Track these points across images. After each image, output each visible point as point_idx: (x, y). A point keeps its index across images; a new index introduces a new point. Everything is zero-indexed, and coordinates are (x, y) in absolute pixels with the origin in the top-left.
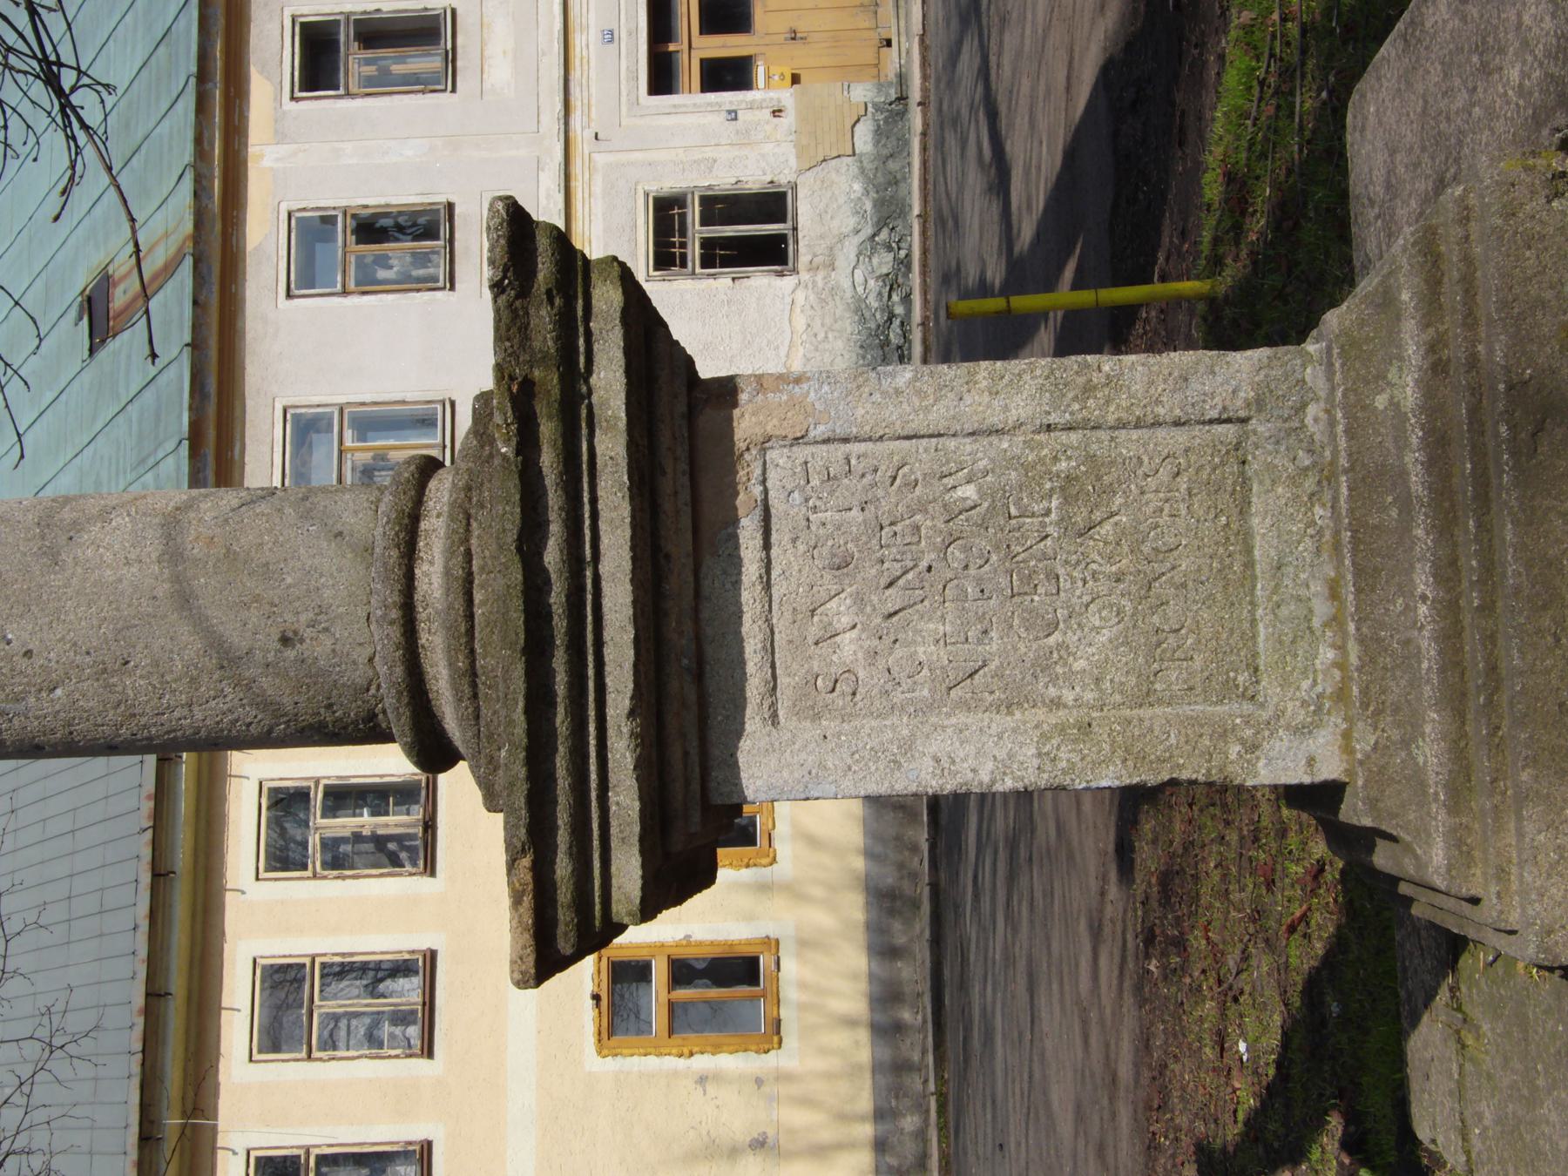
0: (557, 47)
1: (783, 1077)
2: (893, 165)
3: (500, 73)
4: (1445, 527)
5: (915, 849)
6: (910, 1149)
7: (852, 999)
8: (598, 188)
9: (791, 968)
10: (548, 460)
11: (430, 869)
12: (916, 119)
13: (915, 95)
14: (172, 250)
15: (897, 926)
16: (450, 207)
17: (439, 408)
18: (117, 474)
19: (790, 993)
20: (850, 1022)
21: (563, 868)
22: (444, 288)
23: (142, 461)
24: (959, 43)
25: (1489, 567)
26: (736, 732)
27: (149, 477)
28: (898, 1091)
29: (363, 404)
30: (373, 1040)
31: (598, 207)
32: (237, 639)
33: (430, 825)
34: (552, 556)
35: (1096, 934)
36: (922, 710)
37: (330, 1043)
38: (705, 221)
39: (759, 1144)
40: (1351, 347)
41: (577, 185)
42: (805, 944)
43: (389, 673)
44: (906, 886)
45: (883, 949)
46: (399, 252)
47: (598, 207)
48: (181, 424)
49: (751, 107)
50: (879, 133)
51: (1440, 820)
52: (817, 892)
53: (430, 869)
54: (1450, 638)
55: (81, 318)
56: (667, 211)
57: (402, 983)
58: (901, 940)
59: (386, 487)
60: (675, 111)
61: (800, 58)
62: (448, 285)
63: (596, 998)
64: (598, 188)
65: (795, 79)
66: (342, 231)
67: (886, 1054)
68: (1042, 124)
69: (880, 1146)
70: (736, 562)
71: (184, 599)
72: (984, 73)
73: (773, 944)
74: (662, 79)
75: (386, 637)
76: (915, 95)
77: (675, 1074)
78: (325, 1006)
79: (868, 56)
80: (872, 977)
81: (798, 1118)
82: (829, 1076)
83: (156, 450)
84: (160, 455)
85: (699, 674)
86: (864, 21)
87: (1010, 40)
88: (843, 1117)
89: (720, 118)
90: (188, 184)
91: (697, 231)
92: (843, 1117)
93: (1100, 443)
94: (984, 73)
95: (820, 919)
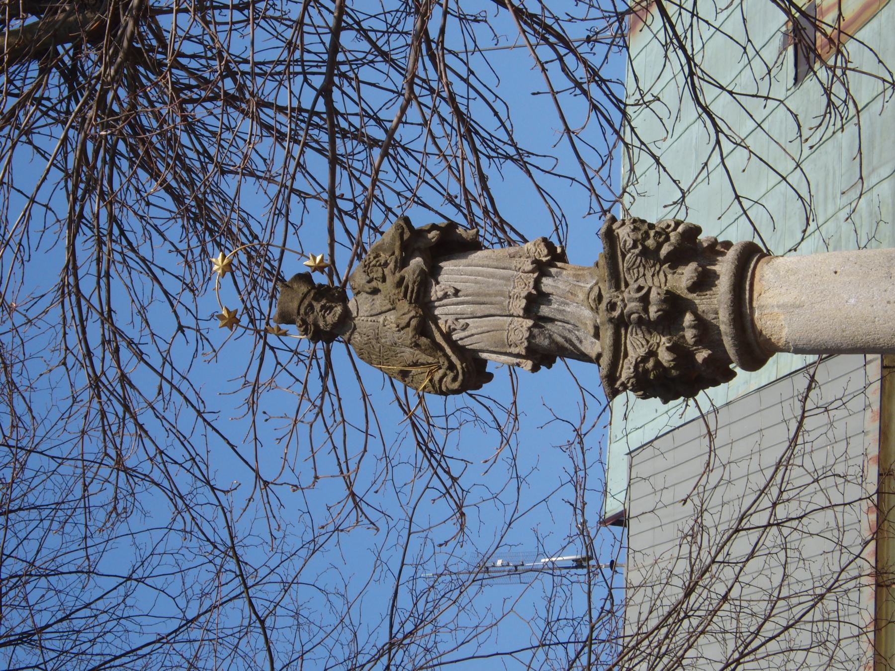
18: (826, 198)
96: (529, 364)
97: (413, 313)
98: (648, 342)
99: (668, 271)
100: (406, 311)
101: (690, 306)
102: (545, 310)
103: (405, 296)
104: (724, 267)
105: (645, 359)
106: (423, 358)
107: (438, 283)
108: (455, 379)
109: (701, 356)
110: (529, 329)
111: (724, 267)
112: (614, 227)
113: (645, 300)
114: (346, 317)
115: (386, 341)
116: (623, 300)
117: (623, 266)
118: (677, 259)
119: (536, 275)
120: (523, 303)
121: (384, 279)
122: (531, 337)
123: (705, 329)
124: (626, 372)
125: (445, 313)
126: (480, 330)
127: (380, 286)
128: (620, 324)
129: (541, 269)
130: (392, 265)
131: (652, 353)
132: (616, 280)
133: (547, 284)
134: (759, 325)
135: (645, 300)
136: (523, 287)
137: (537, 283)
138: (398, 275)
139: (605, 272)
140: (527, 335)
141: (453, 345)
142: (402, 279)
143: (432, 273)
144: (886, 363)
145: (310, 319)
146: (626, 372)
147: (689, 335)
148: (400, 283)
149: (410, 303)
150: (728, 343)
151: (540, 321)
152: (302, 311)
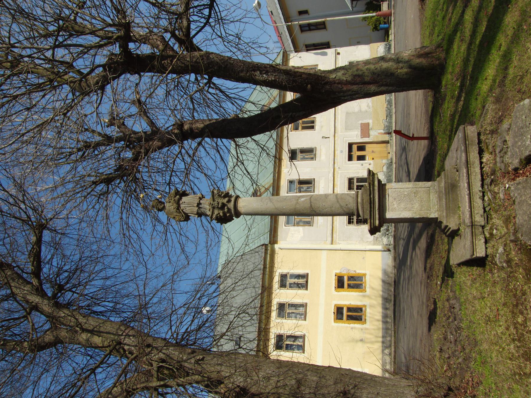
0: (333, 153)
1: (366, 329)
2: (390, 173)
3: (323, 157)
4: (446, 195)
5: (391, 291)
6: (388, 344)
7: (379, 317)
8: (339, 176)
9: (368, 310)
10: (371, 189)
11: (307, 289)
12: (394, 166)
13: (394, 161)
15: (387, 304)
16: (314, 179)
19: (368, 315)
20: (378, 320)
21: (372, 221)
24: (402, 154)
25: (449, 199)
26: (386, 212)
28: (386, 333)
30: (296, 317)
31: (339, 179)
32: (342, 205)
33: (307, 282)
34: (372, 196)
35: (421, 284)
36: (402, 211)
37: (289, 317)
38: (357, 182)
39: (361, 340)
40: (439, 181)
41: (336, 176)
42: (371, 306)
43: (355, 208)
44: (389, 298)
45: (385, 308)
46: (305, 186)
47: (339, 179)
49: (366, 163)
50: (387, 168)
51: (445, 219)
52: (373, 297)
53: (307, 289)
54: (446, 204)
56: (351, 181)
57: (301, 308)
58: (388, 307)
60: (352, 164)
61: (374, 155)
63: (334, 313)
64: (339, 176)
65: (373, 159)
66: (296, 183)
67: (384, 327)
68: (415, 166)
69: (383, 342)
70: (386, 199)
71: (338, 202)
72: (406, 158)
73: (365, 306)
74: (350, 158)
75: (355, 205)
76: (394, 161)
77: (347, 327)
78: (288, 311)
79: (386, 155)
80: (382, 313)
81: (369, 336)
82: (374, 329)
85: (383, 207)
86: (385, 149)
87: (410, 153)
88: (377, 337)
89: (359, 166)
90: (272, 175)
91: (356, 184)
92: (377, 337)
93: (417, 189)
94: (406, 158)
95: (374, 302)
96: (197, 216)
100: (175, 205)
101: (227, 205)
102: (200, 206)
104: (233, 199)
106: (178, 214)
109: (228, 215)
111: (233, 199)
113: (218, 204)
114: (164, 207)
115: (171, 211)
117: (215, 198)
118: (225, 197)
122: (198, 211)
123: (229, 210)
124: (214, 216)
125: (182, 206)
128: (214, 208)
129: (200, 199)
131: (219, 213)
132: (214, 200)
133: (201, 201)
135: (218, 204)
136: (197, 201)
139: (212, 199)
141: (183, 212)
143: (180, 199)
146: (214, 216)
147: (226, 210)
150: (233, 212)
151: (200, 208)
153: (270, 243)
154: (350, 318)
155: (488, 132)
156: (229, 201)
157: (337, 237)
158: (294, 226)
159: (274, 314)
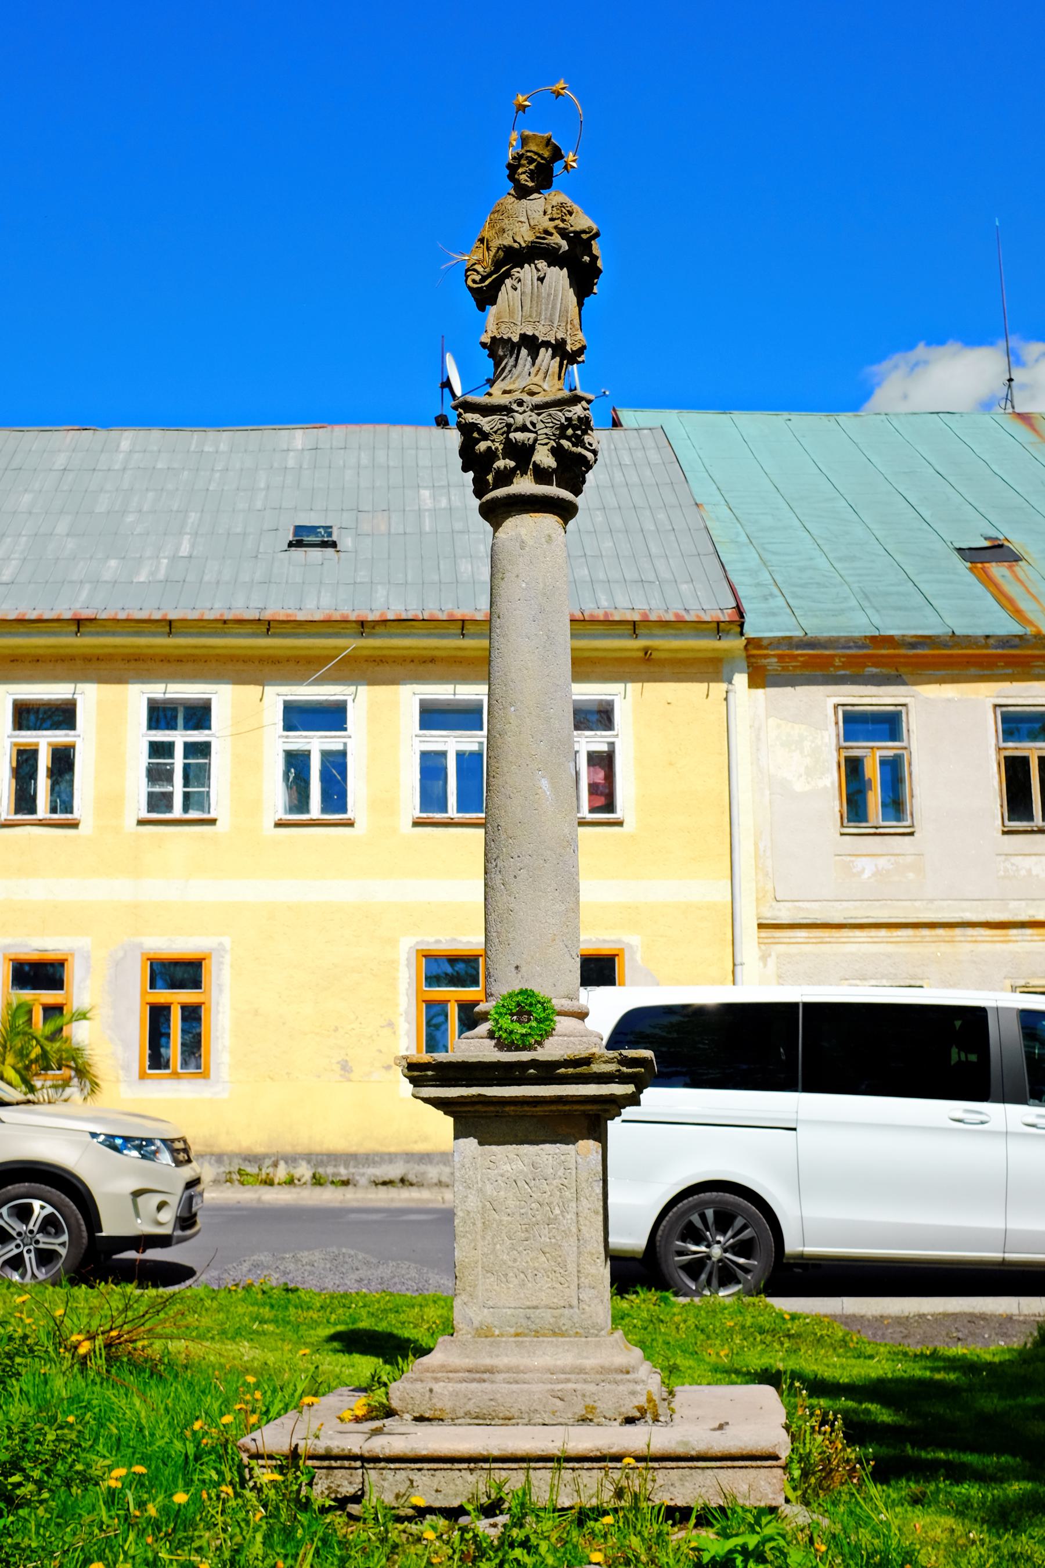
14: (1031, 616)
17: (908, 823)
18: (860, 575)
22: (1003, 825)
23: (866, 597)
27: (853, 603)
29: (910, 764)
48: (891, 629)
55: (986, 539)
59: (484, 1017)
62: (1006, 829)
83: (874, 607)
84: (869, 612)
97: (524, 245)
98: (495, 432)
99: (549, 446)
102: (524, 352)
103: (538, 238)
104: (553, 490)
105: (480, 430)
107: (549, 266)
108: (474, 281)
110: (510, 339)
112: (584, 403)
116: (525, 412)
117: (552, 411)
119: (553, 342)
120: (530, 333)
121: (552, 220)
123: (505, 478)
125: (527, 273)
126: (511, 299)
127: (547, 217)
129: (559, 348)
130: (562, 225)
131: (485, 436)
133: (545, 354)
134: (556, 518)
137: (546, 344)
138: (553, 231)
140: (505, 337)
142: (551, 234)
143: (554, 257)
144: (722, 625)
145: (524, 162)
148: (547, 232)
149: (532, 242)
150: (500, 492)
152: (529, 154)
153: (753, 643)
154: (158, 1015)
155: (425, 1542)
156: (542, 475)
157: (794, 949)
158: (840, 748)
159: (158, 691)
